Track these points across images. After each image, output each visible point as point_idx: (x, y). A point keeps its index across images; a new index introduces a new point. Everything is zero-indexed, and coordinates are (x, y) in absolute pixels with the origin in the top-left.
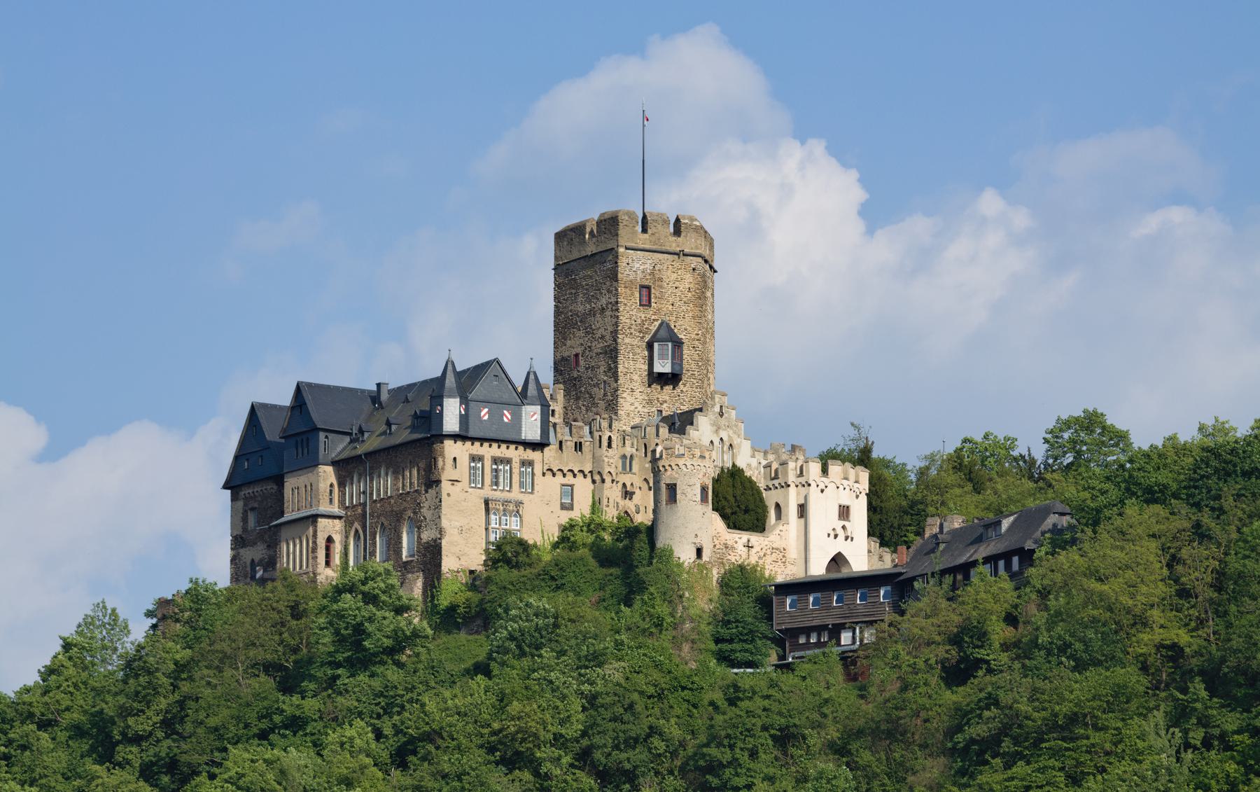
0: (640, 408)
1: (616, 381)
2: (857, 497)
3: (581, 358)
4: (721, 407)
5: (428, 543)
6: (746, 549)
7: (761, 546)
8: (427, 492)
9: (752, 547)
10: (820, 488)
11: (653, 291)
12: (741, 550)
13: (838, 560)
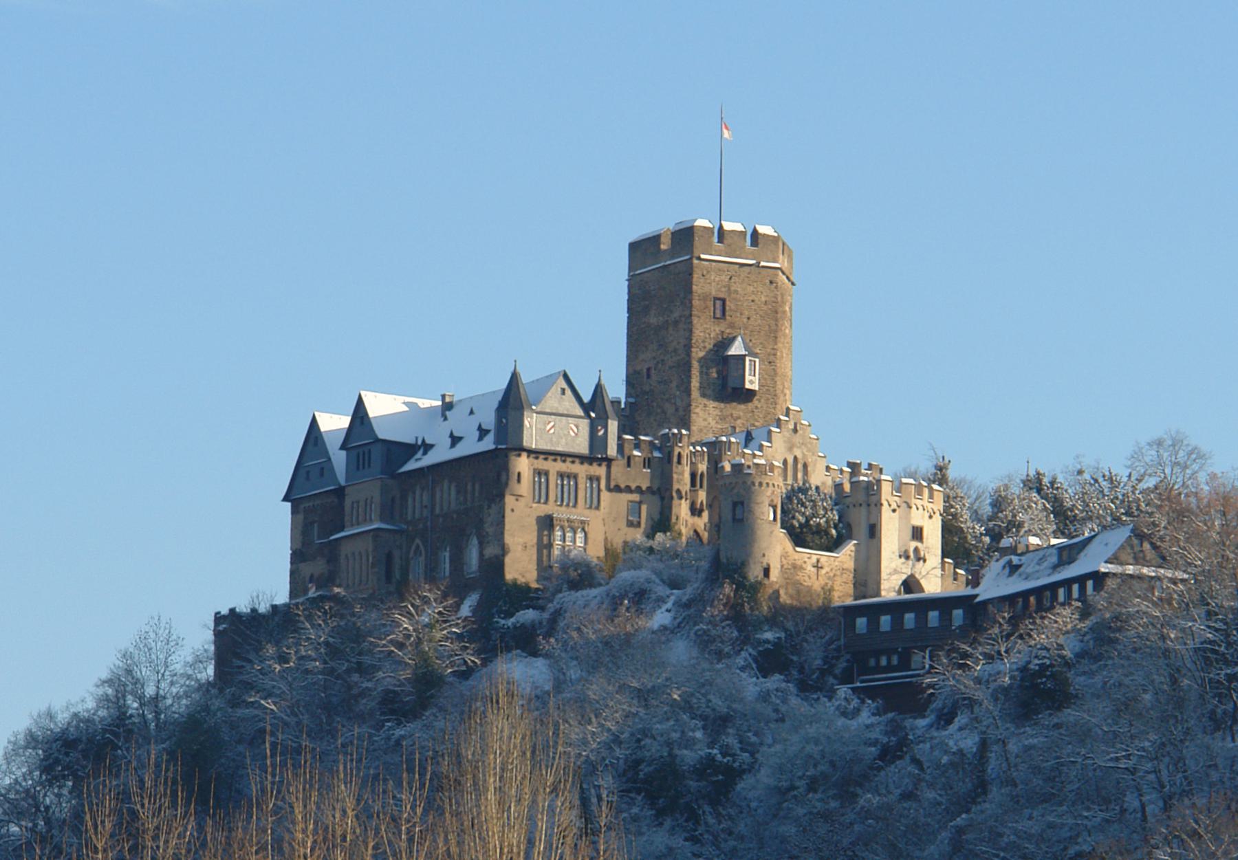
0: (713, 423)
1: (689, 395)
2: (931, 517)
3: (653, 371)
4: (795, 425)
5: (490, 558)
6: (814, 570)
7: (831, 567)
8: (489, 507)
9: (822, 568)
10: (893, 507)
11: (728, 303)
12: (810, 569)
13: (910, 584)
